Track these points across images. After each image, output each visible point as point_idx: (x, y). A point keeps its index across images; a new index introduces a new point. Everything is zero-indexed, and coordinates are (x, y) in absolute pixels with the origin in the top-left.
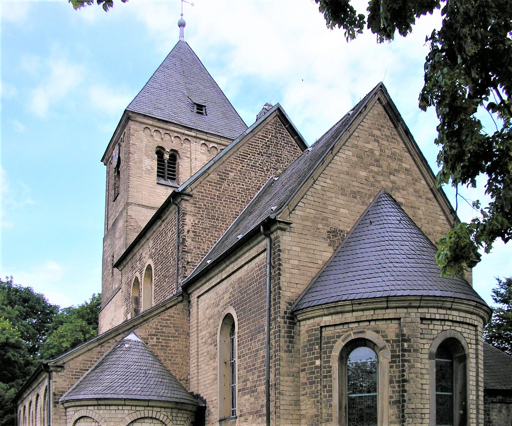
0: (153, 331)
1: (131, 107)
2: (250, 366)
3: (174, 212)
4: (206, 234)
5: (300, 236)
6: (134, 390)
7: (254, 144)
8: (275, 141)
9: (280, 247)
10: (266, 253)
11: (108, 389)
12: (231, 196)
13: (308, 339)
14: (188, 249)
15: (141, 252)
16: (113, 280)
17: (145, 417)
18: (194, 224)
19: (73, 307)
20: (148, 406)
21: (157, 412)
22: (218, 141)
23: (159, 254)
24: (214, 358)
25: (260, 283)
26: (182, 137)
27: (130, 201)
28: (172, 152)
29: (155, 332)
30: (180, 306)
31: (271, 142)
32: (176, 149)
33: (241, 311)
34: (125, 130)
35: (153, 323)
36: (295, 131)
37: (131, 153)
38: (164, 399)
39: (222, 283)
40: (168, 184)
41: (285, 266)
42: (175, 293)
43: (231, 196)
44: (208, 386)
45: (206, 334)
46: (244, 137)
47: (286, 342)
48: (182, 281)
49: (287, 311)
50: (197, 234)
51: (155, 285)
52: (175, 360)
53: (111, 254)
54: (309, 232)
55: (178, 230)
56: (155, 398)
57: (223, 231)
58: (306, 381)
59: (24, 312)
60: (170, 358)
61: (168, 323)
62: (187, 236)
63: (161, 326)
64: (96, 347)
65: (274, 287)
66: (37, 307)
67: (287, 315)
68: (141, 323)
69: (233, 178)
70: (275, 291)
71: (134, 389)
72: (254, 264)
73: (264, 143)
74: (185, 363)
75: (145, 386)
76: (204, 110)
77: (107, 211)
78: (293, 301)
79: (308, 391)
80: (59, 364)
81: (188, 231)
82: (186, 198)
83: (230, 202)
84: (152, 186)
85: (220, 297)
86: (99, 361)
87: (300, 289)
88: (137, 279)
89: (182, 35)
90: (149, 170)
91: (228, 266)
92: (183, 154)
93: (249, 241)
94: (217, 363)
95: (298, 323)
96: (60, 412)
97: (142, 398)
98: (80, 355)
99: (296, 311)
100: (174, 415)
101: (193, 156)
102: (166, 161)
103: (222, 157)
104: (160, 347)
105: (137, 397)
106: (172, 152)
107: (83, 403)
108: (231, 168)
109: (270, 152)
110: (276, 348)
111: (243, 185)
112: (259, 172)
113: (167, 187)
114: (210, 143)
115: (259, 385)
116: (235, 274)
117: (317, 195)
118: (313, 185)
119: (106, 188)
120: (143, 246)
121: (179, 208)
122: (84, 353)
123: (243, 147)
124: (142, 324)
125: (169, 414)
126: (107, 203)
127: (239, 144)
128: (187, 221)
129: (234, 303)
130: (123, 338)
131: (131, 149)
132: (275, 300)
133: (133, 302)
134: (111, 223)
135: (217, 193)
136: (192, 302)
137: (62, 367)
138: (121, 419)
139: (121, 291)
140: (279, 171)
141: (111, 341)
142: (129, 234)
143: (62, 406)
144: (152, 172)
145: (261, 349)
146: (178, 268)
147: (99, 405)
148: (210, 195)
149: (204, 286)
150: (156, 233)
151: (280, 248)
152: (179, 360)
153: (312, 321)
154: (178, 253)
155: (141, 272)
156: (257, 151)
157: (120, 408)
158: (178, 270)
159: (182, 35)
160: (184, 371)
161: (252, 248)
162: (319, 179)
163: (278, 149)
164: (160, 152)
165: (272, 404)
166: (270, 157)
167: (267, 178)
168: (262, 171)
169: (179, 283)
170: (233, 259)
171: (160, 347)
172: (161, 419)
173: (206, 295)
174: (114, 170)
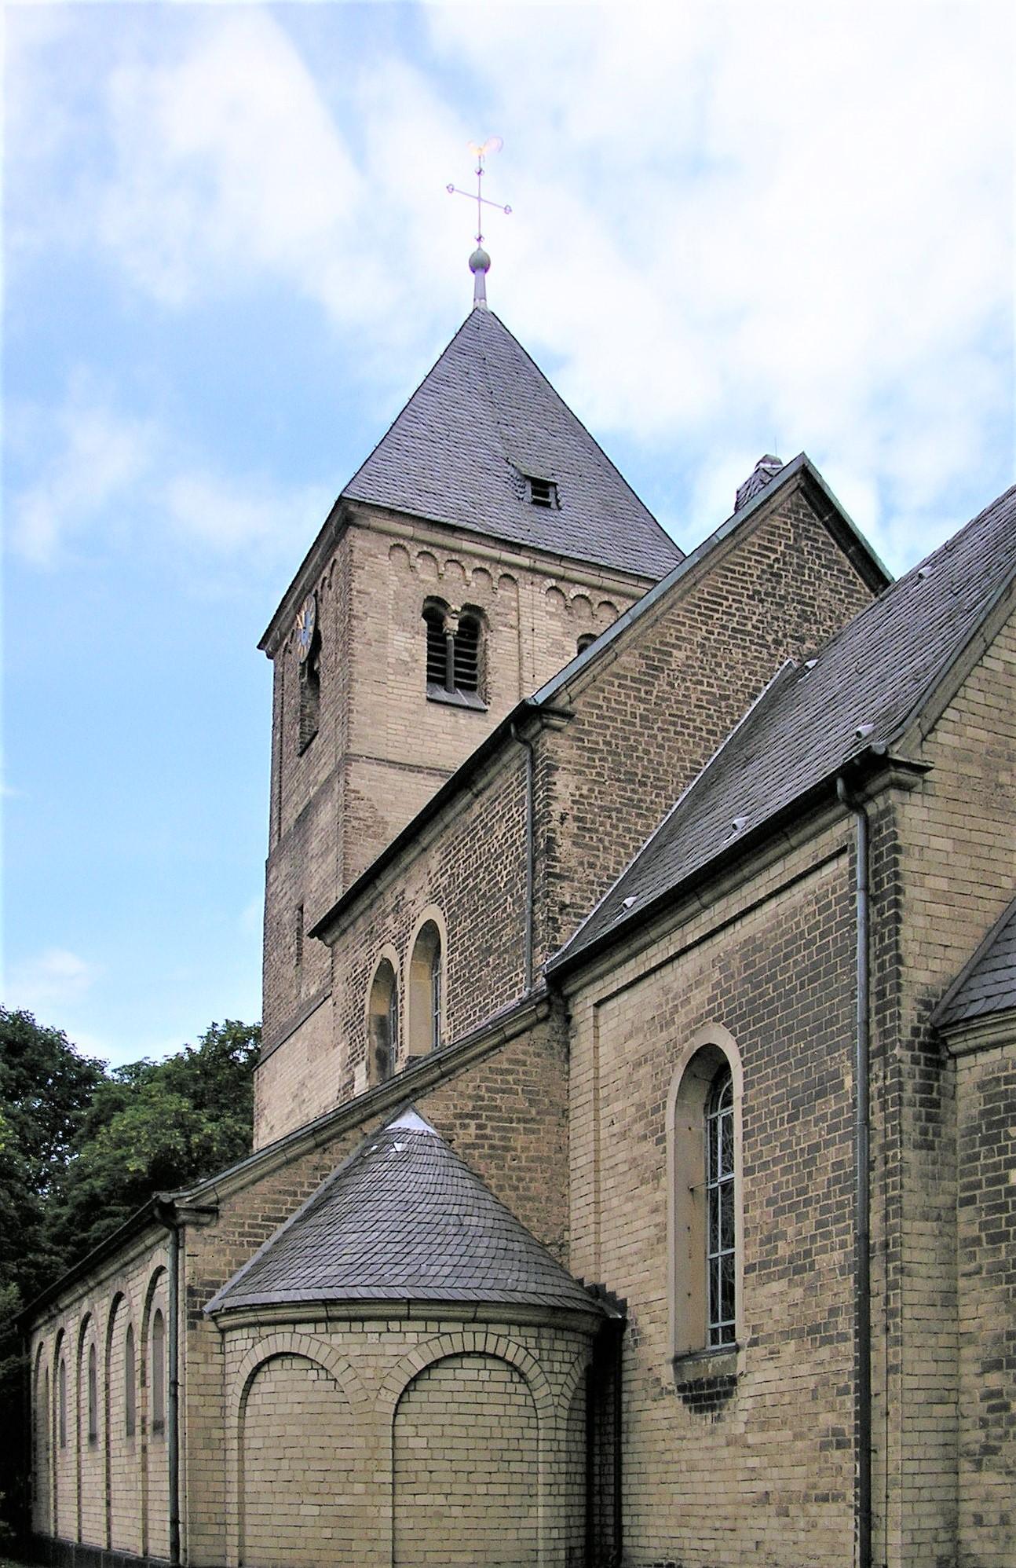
0: (466, 1105)
1: (353, 488)
2: (787, 1196)
3: (516, 764)
4: (612, 826)
5: (952, 806)
6: (432, 1273)
7: (737, 568)
8: (795, 560)
9: (896, 839)
10: (844, 860)
11: (357, 1272)
12: (679, 717)
13: (982, 1107)
14: (561, 868)
15: (399, 889)
16: (300, 975)
17: (464, 1352)
18: (577, 798)
19: (147, 1062)
20: (474, 1320)
21: (499, 1336)
22: (595, 581)
23: (464, 889)
24: (656, 1177)
25: (820, 949)
26: (496, 569)
27: (353, 749)
28: (466, 613)
29: (474, 1108)
30: (543, 1032)
31: (785, 563)
32: (478, 603)
33: (752, 1035)
34: (337, 555)
35: (467, 1082)
36: (851, 530)
37: (355, 617)
38: (518, 1297)
39: (683, 960)
40: (461, 703)
41: (911, 893)
42: (524, 994)
43: (679, 717)
44: (630, 1260)
45: (624, 1110)
46: (713, 550)
47: (918, 1118)
48: (544, 961)
49: (919, 1029)
50: (588, 826)
51: (450, 977)
52: (527, 1189)
53: (295, 902)
54: (975, 797)
55: (533, 816)
56: (495, 1296)
57: (659, 816)
58: (977, 1233)
59: (12, 1079)
60: (515, 1183)
61: (508, 1082)
62: (558, 830)
63: (488, 1090)
64: (309, 1152)
65: (877, 957)
66: (48, 1065)
67: (921, 1038)
68: (433, 1083)
69: (684, 665)
70: (882, 967)
71: (433, 1270)
72: (801, 894)
73: (765, 567)
74: (556, 1196)
75: (463, 1263)
76: (552, 495)
77: (277, 785)
78: (935, 996)
79: (985, 1261)
80: (204, 1202)
81: (563, 819)
82: (556, 722)
83: (676, 733)
84: (413, 707)
85: (674, 999)
86: (316, 1193)
87: (953, 963)
88: (386, 967)
89: (480, 294)
90: (406, 663)
91: (705, 907)
92: (499, 618)
93: (787, 830)
94: (667, 1190)
95: (950, 1063)
96: (206, 1343)
97: (458, 1295)
98: (262, 1177)
99: (945, 1026)
100: (545, 1344)
101: (526, 624)
102: (450, 638)
103: (653, 605)
104: (486, 1151)
105: (444, 1295)
106: (466, 613)
107: (281, 1314)
108: (677, 638)
109: (783, 593)
110: (890, 1138)
111: (709, 685)
112: (753, 647)
113: (455, 711)
114: (570, 585)
115: (823, 1250)
116: (731, 930)
117: (995, 688)
118: (981, 659)
119: (274, 719)
120: (406, 869)
121: (533, 752)
122: (274, 1170)
123: (708, 577)
124: (435, 1086)
125: (532, 1342)
126: (278, 760)
127: (697, 569)
128: (559, 789)
129: (729, 1013)
130: (384, 1126)
131: (356, 605)
132: (881, 994)
133: (373, 1030)
134: (291, 815)
135: (641, 709)
136: (577, 1019)
137: (213, 1211)
138: (395, 1360)
139: (330, 1001)
140: (808, 644)
141: (350, 1135)
142: (352, 843)
143: (211, 1326)
144: (413, 670)
145: (828, 1144)
146: (533, 922)
147: (330, 1319)
148: (621, 714)
149: (619, 972)
150: (450, 832)
151: (897, 842)
152: (538, 1187)
153: (996, 1054)
154: (534, 879)
155: (400, 945)
156: (748, 589)
157: (394, 1325)
158: (533, 929)
159: (480, 294)
160: (553, 1219)
161: (793, 849)
162: (999, 640)
163: (803, 582)
164: (434, 612)
165: (876, 1303)
166: (783, 605)
167: (777, 666)
168: (761, 645)
169: (536, 965)
170: (726, 885)
171: (486, 1151)
172: (509, 1358)
173: (625, 996)
174: (299, 668)
